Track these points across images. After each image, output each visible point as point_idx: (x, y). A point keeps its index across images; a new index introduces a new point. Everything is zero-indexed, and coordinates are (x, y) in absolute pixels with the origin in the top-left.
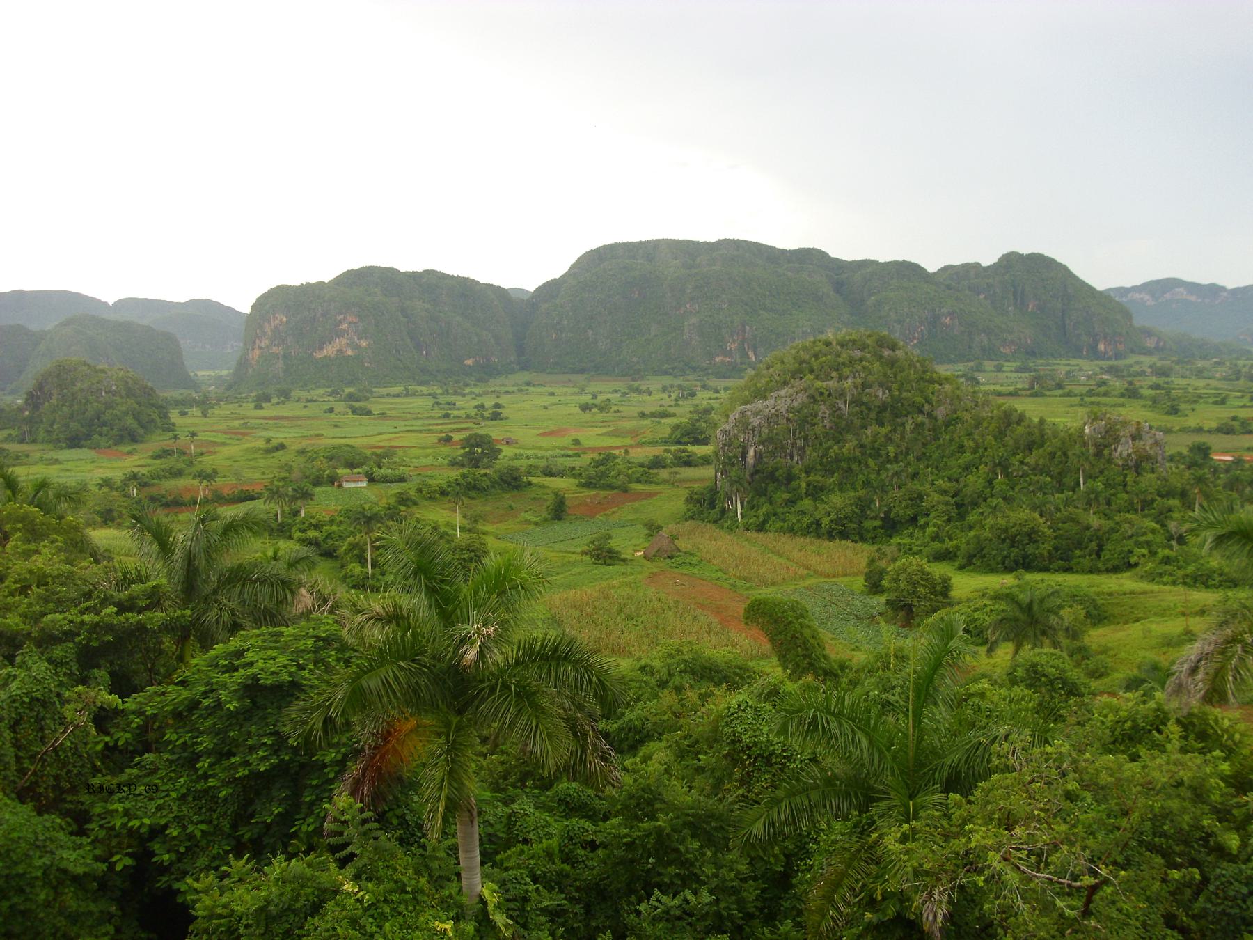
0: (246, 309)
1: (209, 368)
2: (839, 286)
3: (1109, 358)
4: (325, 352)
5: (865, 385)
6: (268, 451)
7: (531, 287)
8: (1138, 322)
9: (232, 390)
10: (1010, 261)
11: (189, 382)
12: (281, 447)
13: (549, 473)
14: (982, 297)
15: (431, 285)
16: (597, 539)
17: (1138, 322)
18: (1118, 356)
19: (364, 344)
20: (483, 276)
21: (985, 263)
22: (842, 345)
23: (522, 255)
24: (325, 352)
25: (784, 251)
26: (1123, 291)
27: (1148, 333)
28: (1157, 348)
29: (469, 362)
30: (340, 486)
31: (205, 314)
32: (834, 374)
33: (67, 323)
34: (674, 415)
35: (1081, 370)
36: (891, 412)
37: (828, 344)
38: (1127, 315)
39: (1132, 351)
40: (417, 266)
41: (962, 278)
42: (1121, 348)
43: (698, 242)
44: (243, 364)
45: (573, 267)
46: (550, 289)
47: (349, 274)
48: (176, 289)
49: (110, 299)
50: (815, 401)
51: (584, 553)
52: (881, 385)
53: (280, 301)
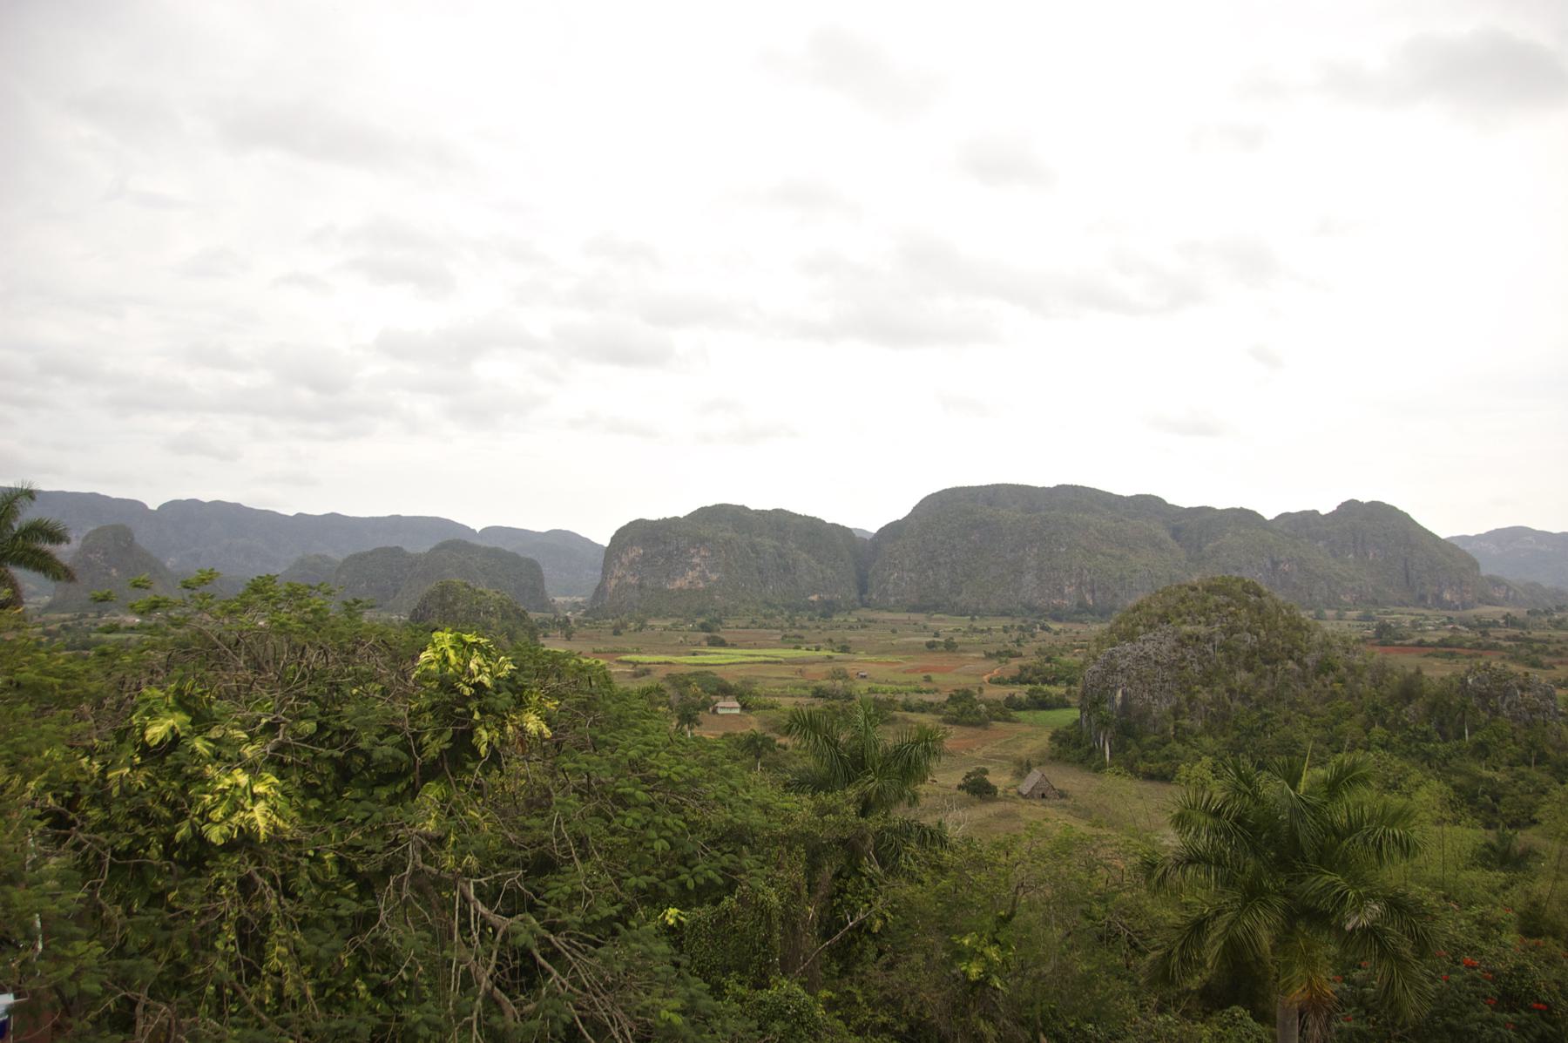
0: (606, 543)
1: (566, 594)
2: (1176, 533)
3: (1457, 608)
4: (678, 583)
5: (1232, 630)
6: (636, 675)
7: (873, 528)
8: (1485, 571)
9: (596, 611)
10: (1350, 509)
11: (544, 605)
12: (647, 672)
13: (908, 708)
14: (1320, 544)
15: (780, 523)
16: (974, 774)
17: (1485, 571)
18: (1465, 606)
19: (714, 577)
20: (829, 518)
21: (1323, 512)
22: (1210, 589)
23: (867, 501)
24: (678, 583)
25: (1121, 497)
26: (1465, 539)
27: (1496, 582)
28: (1506, 598)
29: (814, 598)
30: (714, 711)
31: (564, 544)
32: (1202, 619)
33: (443, 546)
34: (1020, 655)
35: (1427, 618)
36: (1264, 657)
37: (1194, 589)
38: (1475, 565)
39: (1480, 601)
40: (768, 506)
41: (1301, 524)
42: (1469, 597)
43: (1110, 494)
44: (600, 590)
45: (915, 509)
46: (892, 531)
47: (702, 510)
48: (537, 519)
49: (478, 527)
50: (1184, 645)
51: (960, 787)
52: (1249, 630)
53: (636, 534)
